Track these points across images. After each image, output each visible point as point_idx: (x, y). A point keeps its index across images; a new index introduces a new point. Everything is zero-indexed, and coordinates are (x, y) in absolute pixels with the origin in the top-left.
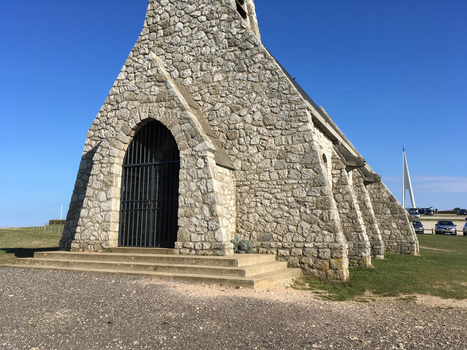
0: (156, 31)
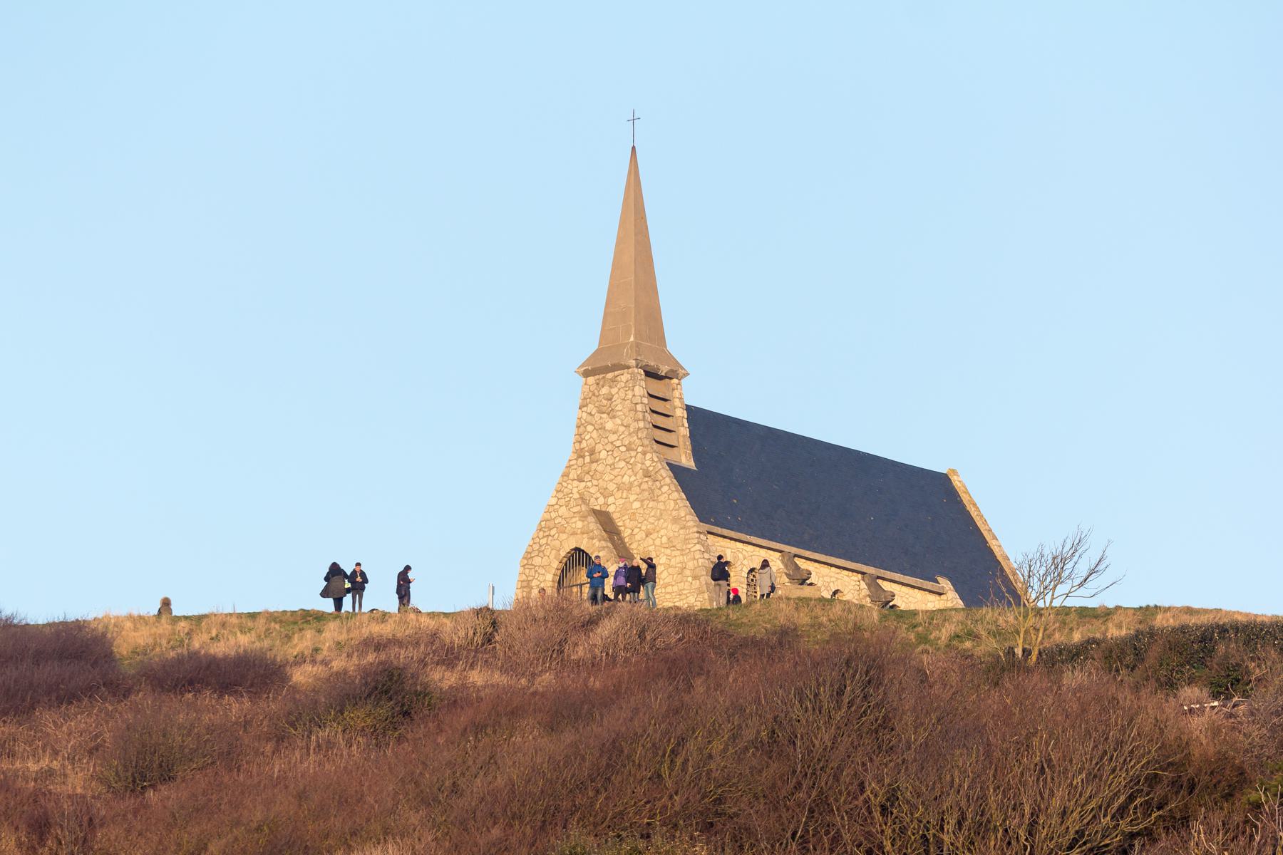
0: (583, 457)
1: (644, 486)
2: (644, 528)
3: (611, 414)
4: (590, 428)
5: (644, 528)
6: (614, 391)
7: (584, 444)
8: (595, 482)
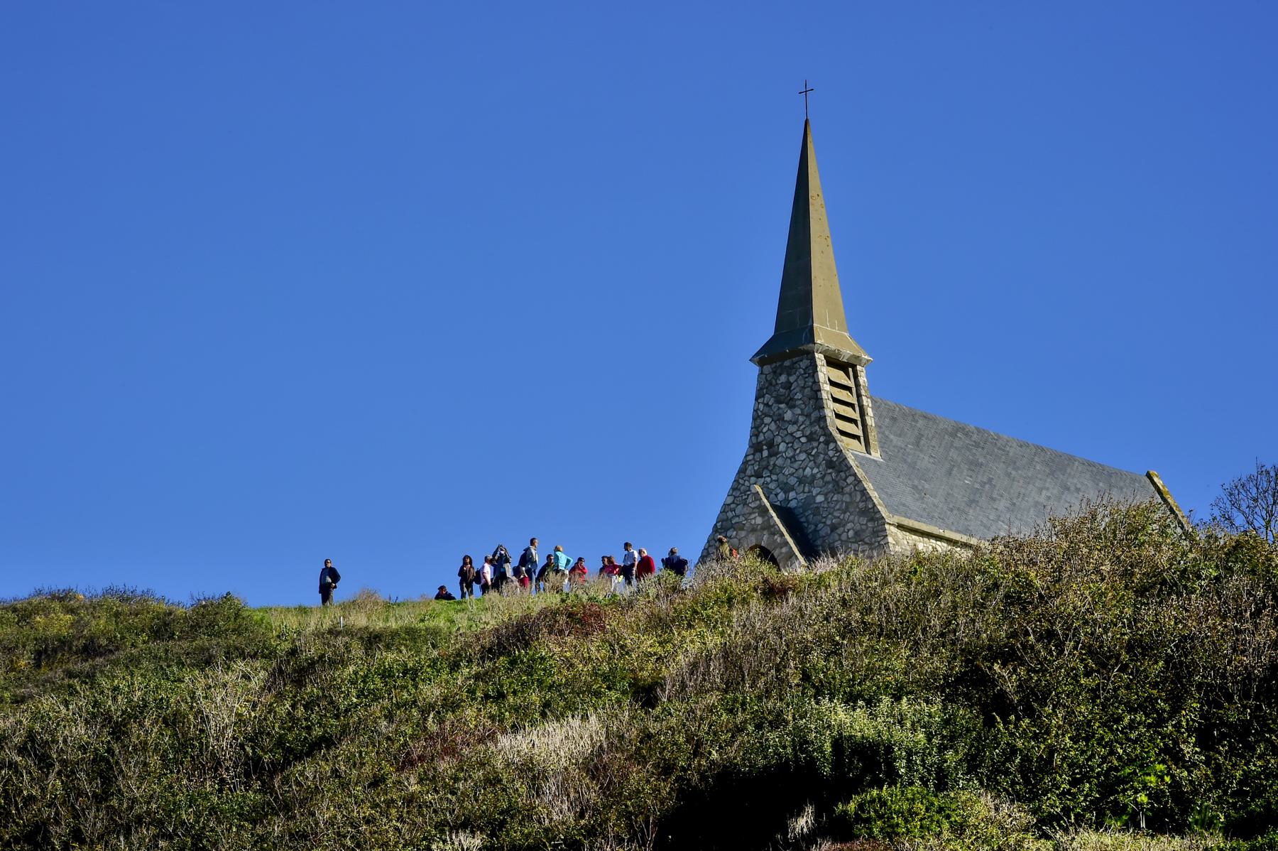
1: (828, 478)
2: (829, 522)
3: (791, 404)
4: (767, 420)
5: (829, 522)
6: (792, 379)
7: (761, 437)
8: (774, 477)
